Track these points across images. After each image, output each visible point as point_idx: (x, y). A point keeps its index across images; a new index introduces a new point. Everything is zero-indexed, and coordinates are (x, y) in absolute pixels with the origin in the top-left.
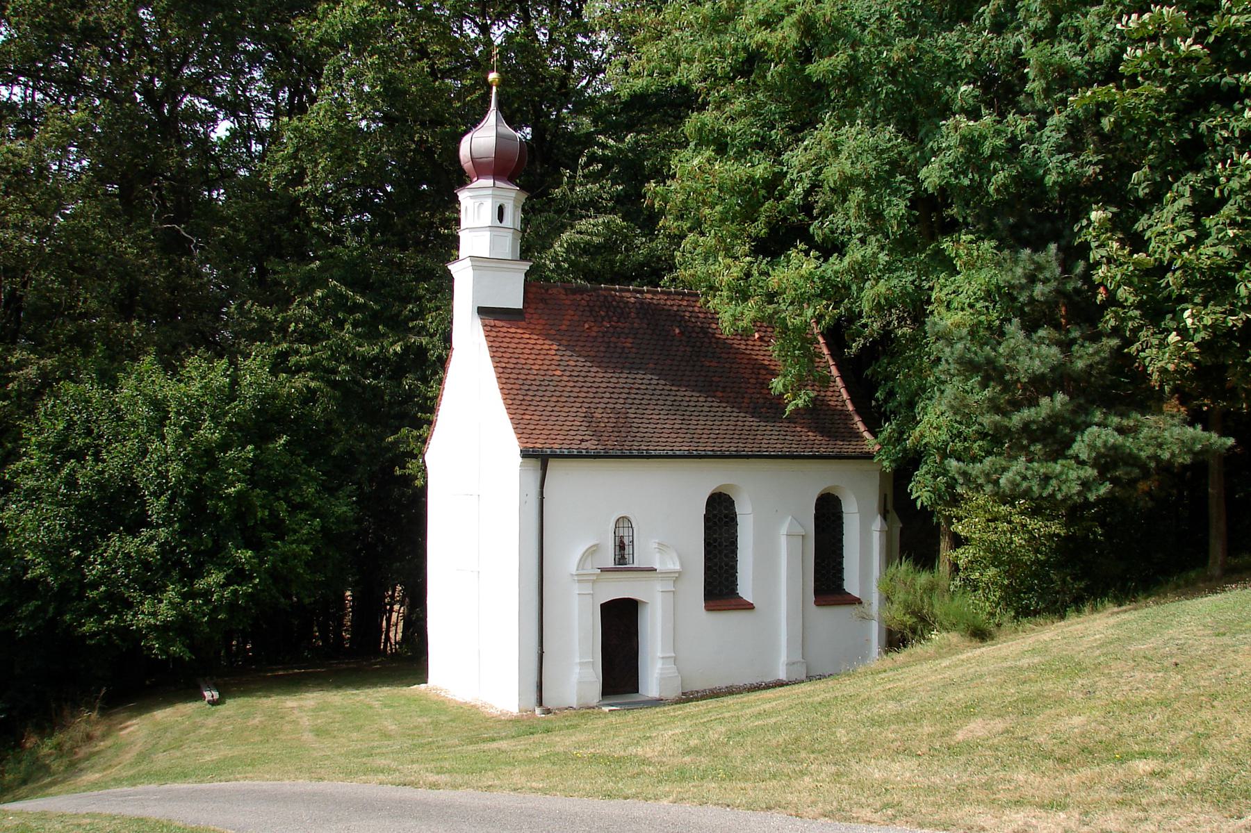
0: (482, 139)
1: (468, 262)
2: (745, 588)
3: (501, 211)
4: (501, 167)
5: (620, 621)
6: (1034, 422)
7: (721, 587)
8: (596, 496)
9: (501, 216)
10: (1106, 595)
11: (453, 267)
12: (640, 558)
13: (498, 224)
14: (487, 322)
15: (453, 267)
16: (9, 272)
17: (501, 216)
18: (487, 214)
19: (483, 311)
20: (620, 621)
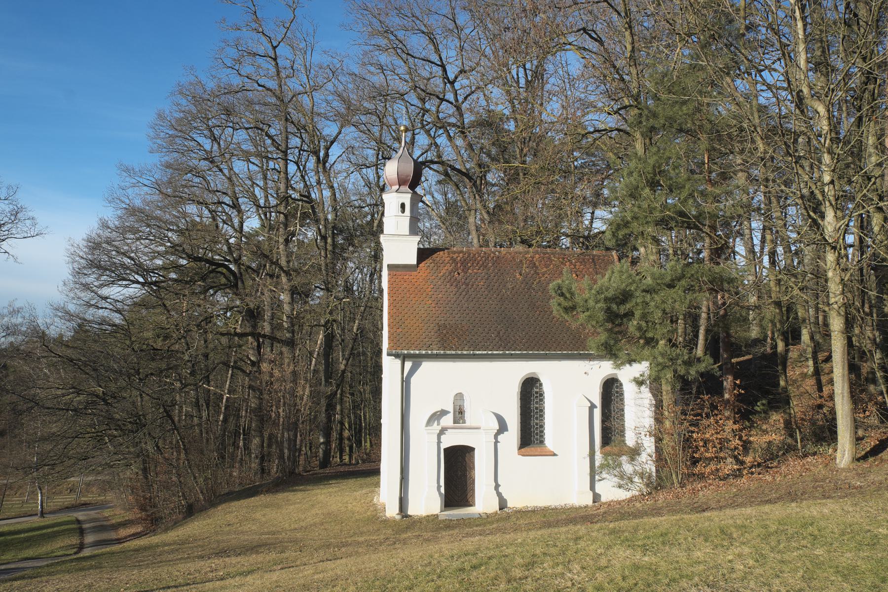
3: (403, 206)
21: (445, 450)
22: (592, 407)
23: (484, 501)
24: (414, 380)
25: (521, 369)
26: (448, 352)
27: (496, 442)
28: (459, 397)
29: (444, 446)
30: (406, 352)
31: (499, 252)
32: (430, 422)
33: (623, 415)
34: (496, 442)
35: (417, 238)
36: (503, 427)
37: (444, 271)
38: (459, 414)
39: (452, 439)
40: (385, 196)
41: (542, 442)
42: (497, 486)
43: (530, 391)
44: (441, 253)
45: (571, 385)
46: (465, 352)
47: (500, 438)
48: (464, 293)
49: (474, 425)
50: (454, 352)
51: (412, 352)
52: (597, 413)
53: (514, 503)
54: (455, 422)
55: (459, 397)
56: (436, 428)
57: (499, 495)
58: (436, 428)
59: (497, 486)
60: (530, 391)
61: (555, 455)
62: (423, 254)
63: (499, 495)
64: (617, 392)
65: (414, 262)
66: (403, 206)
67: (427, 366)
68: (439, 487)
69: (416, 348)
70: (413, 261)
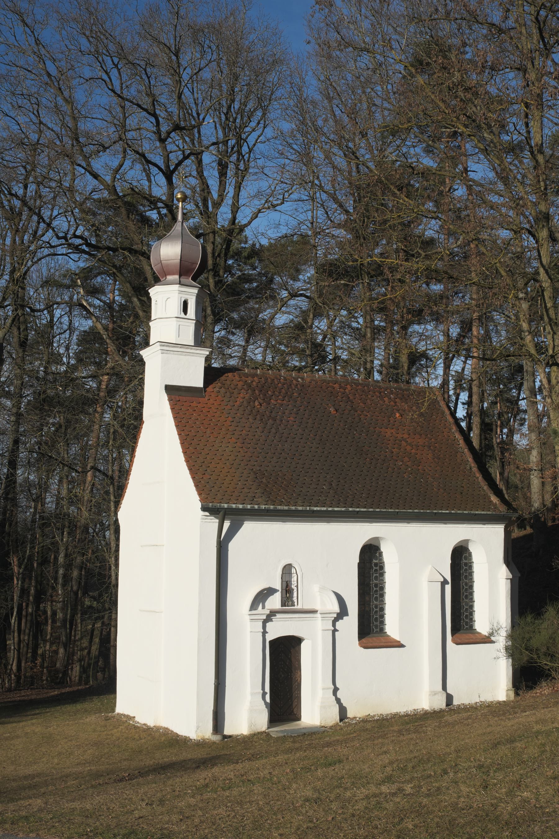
0: (169, 251)
1: (157, 347)
2: (392, 627)
3: (185, 304)
4: (187, 271)
5: (283, 657)
6: (531, 493)
7: (371, 627)
8: (268, 546)
9: (185, 310)
10: (546, 604)
11: (145, 353)
12: (302, 601)
13: (183, 315)
14: (173, 397)
15: (145, 353)
16: (557, 703)
17: (185, 310)
18: (175, 308)
19: (170, 390)
20: (283, 657)
21: (271, 642)
22: (444, 583)
23: (315, 710)
24: (233, 546)
25: (360, 533)
26: (279, 507)
27: (335, 631)
28: (287, 570)
29: (270, 637)
30: (226, 506)
31: (303, 379)
32: (254, 606)
33: (382, 616)
34: (335, 631)
35: (206, 352)
36: (343, 612)
37: (239, 400)
38: (288, 592)
39: (279, 629)
40: (155, 292)
41: (382, 630)
42: (336, 690)
43: (370, 560)
44: (230, 375)
45: (415, 552)
46: (300, 508)
47: (339, 624)
48: (273, 430)
49: (307, 607)
50: (286, 508)
51: (234, 506)
52: (448, 588)
53: (355, 711)
54: (283, 604)
55: (287, 570)
56: (262, 612)
57: (338, 701)
58: (262, 612)
59: (336, 690)
60: (370, 560)
61: (402, 646)
62: (211, 374)
63: (338, 701)
64: (376, 585)
65: (201, 385)
66: (185, 304)
67: (250, 528)
68: (264, 694)
69: (237, 502)
70: (199, 382)
